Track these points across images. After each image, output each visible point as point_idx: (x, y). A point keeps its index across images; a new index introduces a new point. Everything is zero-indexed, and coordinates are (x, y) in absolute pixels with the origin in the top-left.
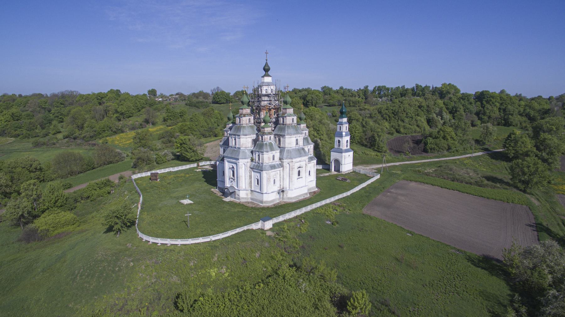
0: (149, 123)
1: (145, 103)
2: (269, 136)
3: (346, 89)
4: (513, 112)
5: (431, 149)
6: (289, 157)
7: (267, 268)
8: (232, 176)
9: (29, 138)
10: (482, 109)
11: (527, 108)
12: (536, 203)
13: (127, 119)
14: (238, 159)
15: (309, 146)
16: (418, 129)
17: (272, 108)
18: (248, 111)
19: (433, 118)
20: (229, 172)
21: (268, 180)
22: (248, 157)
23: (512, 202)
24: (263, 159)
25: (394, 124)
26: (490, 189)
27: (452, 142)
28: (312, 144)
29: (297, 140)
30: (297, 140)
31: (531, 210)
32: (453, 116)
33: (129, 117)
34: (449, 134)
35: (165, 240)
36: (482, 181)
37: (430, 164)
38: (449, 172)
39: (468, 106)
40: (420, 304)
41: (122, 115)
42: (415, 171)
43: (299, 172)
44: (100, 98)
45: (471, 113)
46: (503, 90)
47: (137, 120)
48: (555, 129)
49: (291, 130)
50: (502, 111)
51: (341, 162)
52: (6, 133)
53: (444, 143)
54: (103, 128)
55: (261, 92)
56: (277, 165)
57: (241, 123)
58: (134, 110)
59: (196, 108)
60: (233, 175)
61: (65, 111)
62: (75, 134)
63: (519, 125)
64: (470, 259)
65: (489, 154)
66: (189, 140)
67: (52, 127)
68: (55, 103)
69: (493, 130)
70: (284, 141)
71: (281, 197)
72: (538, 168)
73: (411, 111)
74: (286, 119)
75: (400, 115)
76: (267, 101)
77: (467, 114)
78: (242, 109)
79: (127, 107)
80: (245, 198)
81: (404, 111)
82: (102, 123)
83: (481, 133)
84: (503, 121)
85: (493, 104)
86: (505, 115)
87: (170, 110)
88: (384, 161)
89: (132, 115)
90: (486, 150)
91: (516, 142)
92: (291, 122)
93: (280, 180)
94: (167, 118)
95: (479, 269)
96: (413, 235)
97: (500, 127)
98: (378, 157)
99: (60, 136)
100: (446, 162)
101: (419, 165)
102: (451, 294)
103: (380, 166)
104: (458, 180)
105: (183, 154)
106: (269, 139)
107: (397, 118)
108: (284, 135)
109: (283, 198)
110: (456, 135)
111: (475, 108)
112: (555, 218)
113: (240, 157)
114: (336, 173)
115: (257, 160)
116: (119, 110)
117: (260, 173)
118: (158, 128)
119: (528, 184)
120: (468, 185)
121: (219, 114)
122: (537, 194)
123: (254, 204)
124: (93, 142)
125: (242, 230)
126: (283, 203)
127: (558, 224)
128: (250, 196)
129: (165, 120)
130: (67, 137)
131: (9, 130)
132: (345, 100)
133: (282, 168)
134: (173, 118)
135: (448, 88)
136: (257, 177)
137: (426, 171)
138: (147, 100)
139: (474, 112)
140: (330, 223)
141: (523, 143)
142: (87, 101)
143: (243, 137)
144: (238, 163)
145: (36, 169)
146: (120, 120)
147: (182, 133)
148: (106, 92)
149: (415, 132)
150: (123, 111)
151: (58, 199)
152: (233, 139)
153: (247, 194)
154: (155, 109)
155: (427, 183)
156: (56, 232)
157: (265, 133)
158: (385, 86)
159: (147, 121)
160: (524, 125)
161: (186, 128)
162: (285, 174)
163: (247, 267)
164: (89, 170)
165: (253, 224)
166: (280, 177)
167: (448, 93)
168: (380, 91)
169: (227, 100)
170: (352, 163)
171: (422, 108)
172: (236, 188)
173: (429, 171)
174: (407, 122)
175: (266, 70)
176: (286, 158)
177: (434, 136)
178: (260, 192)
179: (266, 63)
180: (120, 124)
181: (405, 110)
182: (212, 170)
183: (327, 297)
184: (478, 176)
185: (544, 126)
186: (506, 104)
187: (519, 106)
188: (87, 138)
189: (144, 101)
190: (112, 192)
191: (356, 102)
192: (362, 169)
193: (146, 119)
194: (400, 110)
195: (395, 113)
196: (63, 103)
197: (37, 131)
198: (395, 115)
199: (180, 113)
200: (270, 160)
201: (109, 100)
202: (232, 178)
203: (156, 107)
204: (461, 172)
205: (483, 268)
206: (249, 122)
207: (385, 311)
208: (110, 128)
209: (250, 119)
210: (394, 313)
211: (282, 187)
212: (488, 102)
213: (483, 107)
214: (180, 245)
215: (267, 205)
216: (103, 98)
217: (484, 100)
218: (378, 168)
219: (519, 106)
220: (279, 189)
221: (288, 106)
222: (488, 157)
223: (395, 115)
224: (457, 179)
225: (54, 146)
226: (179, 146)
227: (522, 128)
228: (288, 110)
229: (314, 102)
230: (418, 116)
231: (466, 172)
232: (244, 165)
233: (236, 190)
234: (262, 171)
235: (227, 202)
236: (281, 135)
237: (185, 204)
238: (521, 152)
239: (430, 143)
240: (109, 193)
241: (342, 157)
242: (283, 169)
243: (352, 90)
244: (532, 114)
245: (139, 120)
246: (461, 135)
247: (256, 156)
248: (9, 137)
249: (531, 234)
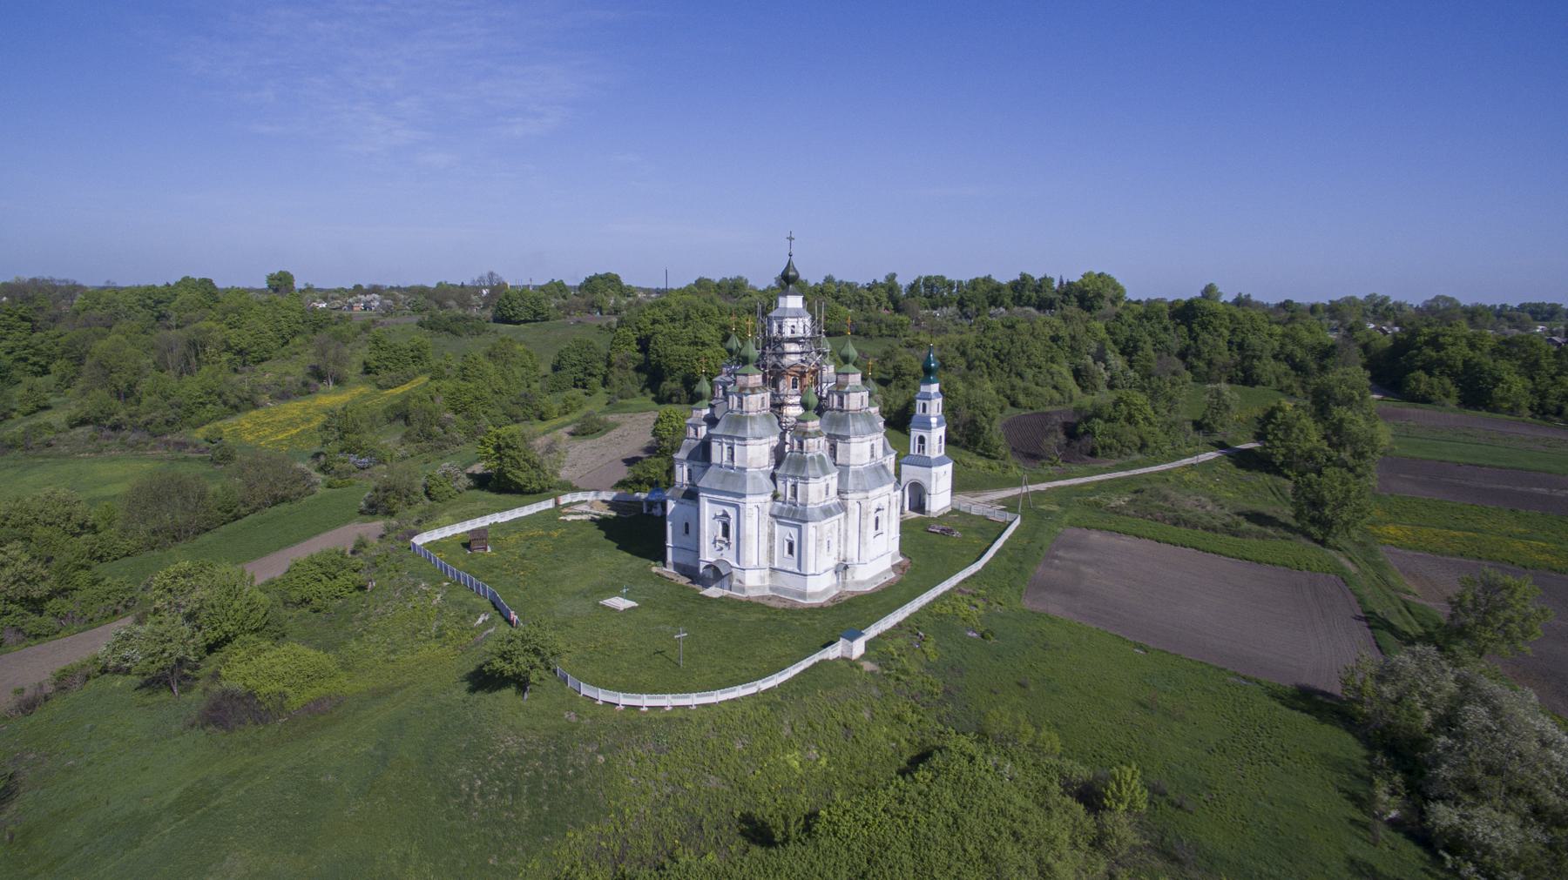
1: (301, 321)
3: (841, 282)
4: (1262, 351)
5: (1103, 448)
6: (860, 487)
7: (898, 742)
8: (720, 537)
10: (1192, 342)
11: (1287, 340)
12: (1353, 569)
16: (1057, 396)
18: (756, 379)
19: (1086, 366)
21: (818, 541)
22: (766, 490)
23: (1307, 569)
24: (806, 494)
25: (1001, 384)
26: (1255, 540)
27: (1149, 429)
29: (872, 446)
31: (1347, 585)
32: (1129, 361)
34: (1140, 410)
35: (633, 697)
36: (1238, 524)
37: (1114, 486)
38: (1161, 503)
39: (1162, 335)
40: (1218, 787)
42: (1089, 504)
45: (1169, 355)
46: (1211, 285)
48: (1358, 398)
49: (860, 425)
50: (1234, 348)
51: (926, 486)
53: (1130, 434)
55: (780, 332)
57: (744, 409)
59: (451, 336)
60: (726, 533)
63: (1274, 382)
64: (1274, 695)
65: (1229, 456)
69: (1231, 399)
70: (848, 451)
72: (1349, 491)
73: (1038, 349)
74: (848, 399)
75: (1015, 360)
76: (796, 353)
77: (1160, 358)
78: (746, 375)
79: (253, 332)
80: (758, 588)
81: (1024, 352)
82: (192, 385)
83: (1206, 406)
84: (1240, 374)
85: (1216, 331)
86: (1244, 359)
87: (384, 342)
89: (267, 356)
90: (1221, 445)
91: (1288, 428)
94: (376, 364)
95: (1296, 713)
96: (1147, 652)
97: (1235, 386)
98: (995, 472)
100: (1147, 478)
101: (1090, 488)
102: (1263, 763)
103: (1017, 491)
104: (1186, 523)
105: (509, 475)
106: (817, 446)
107: (1008, 370)
109: (844, 583)
110: (1156, 413)
111: (1177, 340)
112: (1390, 598)
113: (749, 489)
114: (915, 515)
115: (789, 496)
118: (356, 392)
119: (1331, 528)
120: (1210, 534)
121: (528, 352)
122: (1347, 549)
123: (785, 601)
124: (177, 438)
126: (849, 596)
127: (1400, 612)
128: (767, 583)
129: (367, 370)
130: (83, 422)
132: (868, 320)
133: (843, 514)
134: (396, 364)
135: (1100, 285)
136: (788, 537)
137: (1112, 505)
139: (1176, 351)
140: (975, 635)
141: (1302, 431)
143: (753, 442)
144: (741, 505)
145: (82, 526)
147: (456, 412)
149: (1051, 402)
150: (244, 345)
152: (725, 446)
153: (762, 579)
155: (1125, 533)
157: (809, 433)
158: (942, 278)
159: (318, 374)
160: (1286, 382)
161: (467, 398)
163: (858, 742)
166: (839, 535)
167: (1099, 296)
168: (932, 291)
169: (536, 314)
171: (1059, 343)
172: (734, 564)
173: (1118, 503)
174: (1030, 377)
176: (854, 491)
177: (1106, 416)
178: (797, 571)
180: (243, 382)
181: (1025, 348)
182: (614, 517)
183: (1056, 788)
184: (1223, 511)
185: (1336, 390)
186: (1243, 332)
187: (1271, 335)
188: (157, 427)
189: (297, 315)
190: (370, 586)
191: (895, 325)
192: (981, 504)
193: (313, 367)
194: (1013, 350)
195: (1002, 357)
196: (30, 315)
198: (1002, 362)
200: (821, 497)
202: (720, 541)
204: (1187, 503)
205: (1303, 711)
207: (1163, 804)
210: (1179, 807)
211: (842, 557)
212: (1204, 326)
213: (1195, 339)
214: (694, 707)
215: (816, 601)
216: (162, 302)
218: (1004, 499)
219: (1271, 335)
220: (836, 562)
221: (851, 367)
222: (1229, 464)
223: (1002, 362)
224: (1184, 521)
225: (46, 451)
226: (493, 452)
227: (1281, 390)
228: (851, 377)
230: (1053, 362)
231: (1196, 503)
232: (756, 509)
233: (733, 570)
234: (806, 522)
235: (716, 599)
236: (838, 437)
237: (622, 609)
238: (1298, 452)
239: (1102, 434)
240: (362, 588)
241: (930, 476)
242: (846, 516)
243: (857, 284)
244: (1299, 355)
246: (1165, 412)
247: (785, 488)
249: (1361, 632)
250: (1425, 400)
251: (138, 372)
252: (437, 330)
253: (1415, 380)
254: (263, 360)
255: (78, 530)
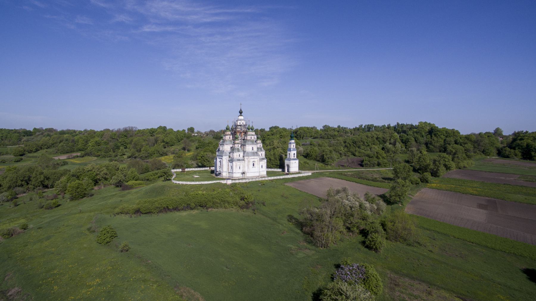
0: (186, 150)
2: (237, 145)
8: (220, 166)
9: (105, 157)
13: (171, 147)
14: (222, 156)
15: (262, 152)
17: (242, 132)
18: (230, 133)
20: (219, 164)
21: (236, 166)
24: (234, 156)
28: (263, 151)
29: (253, 148)
30: (253, 148)
33: (171, 146)
41: (167, 144)
43: (254, 164)
44: (152, 132)
46: (498, 128)
47: (177, 148)
49: (250, 143)
52: (92, 154)
54: (154, 152)
56: (242, 159)
58: (175, 140)
60: (221, 165)
61: (128, 141)
62: (136, 154)
66: (206, 154)
67: (120, 151)
68: (121, 135)
70: (246, 148)
71: (244, 176)
84: (443, 149)
88: (317, 168)
89: (174, 144)
92: (250, 139)
93: (243, 167)
94: (199, 146)
99: (125, 157)
108: (246, 145)
109: (244, 177)
115: (231, 156)
116: (165, 140)
117: (232, 163)
124: (147, 160)
125: (216, 182)
130: (129, 158)
131: (94, 152)
138: (185, 134)
142: (143, 134)
146: (165, 148)
148: (156, 128)
150: (168, 141)
151: (135, 177)
153: (226, 174)
154: (191, 141)
156: (136, 186)
162: (245, 165)
164: (146, 173)
165: (222, 181)
166: (243, 166)
170: (298, 168)
175: (241, 112)
176: (246, 156)
179: (241, 109)
180: (165, 150)
189: (183, 135)
193: (183, 147)
197: (110, 153)
199: (208, 144)
201: (159, 133)
203: (192, 139)
206: (230, 138)
208: (158, 152)
209: (230, 137)
211: (244, 171)
216: (154, 132)
217: (433, 133)
225: (121, 162)
229: (302, 136)
232: (225, 159)
234: (233, 161)
245: (178, 148)
248: (94, 157)
250: (507, 157)
251: (142, 146)
252: (217, 139)
253: (505, 150)
254: (172, 145)
255: (117, 170)
